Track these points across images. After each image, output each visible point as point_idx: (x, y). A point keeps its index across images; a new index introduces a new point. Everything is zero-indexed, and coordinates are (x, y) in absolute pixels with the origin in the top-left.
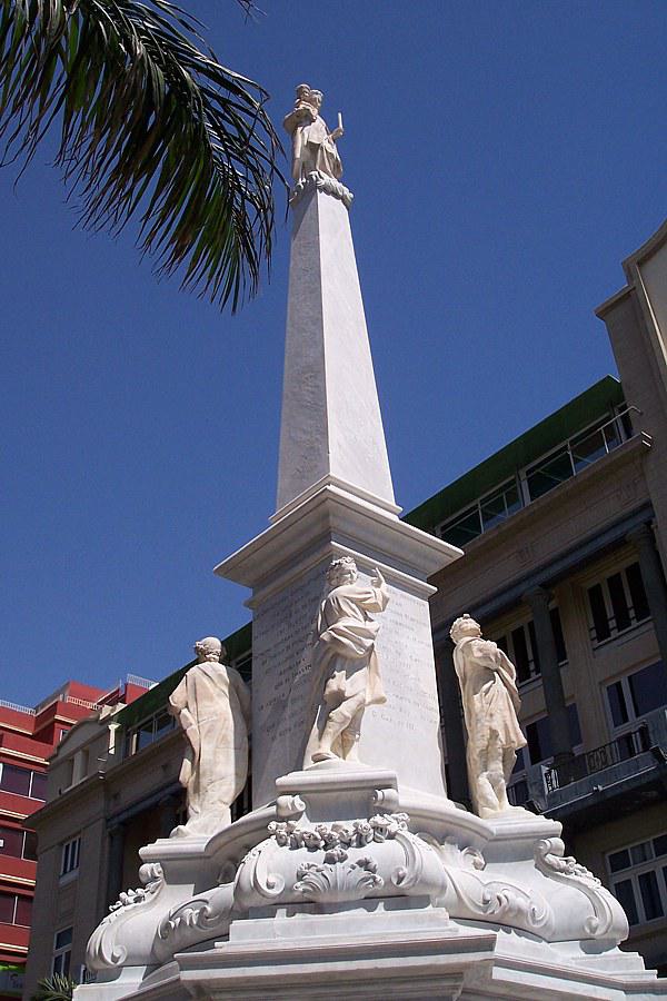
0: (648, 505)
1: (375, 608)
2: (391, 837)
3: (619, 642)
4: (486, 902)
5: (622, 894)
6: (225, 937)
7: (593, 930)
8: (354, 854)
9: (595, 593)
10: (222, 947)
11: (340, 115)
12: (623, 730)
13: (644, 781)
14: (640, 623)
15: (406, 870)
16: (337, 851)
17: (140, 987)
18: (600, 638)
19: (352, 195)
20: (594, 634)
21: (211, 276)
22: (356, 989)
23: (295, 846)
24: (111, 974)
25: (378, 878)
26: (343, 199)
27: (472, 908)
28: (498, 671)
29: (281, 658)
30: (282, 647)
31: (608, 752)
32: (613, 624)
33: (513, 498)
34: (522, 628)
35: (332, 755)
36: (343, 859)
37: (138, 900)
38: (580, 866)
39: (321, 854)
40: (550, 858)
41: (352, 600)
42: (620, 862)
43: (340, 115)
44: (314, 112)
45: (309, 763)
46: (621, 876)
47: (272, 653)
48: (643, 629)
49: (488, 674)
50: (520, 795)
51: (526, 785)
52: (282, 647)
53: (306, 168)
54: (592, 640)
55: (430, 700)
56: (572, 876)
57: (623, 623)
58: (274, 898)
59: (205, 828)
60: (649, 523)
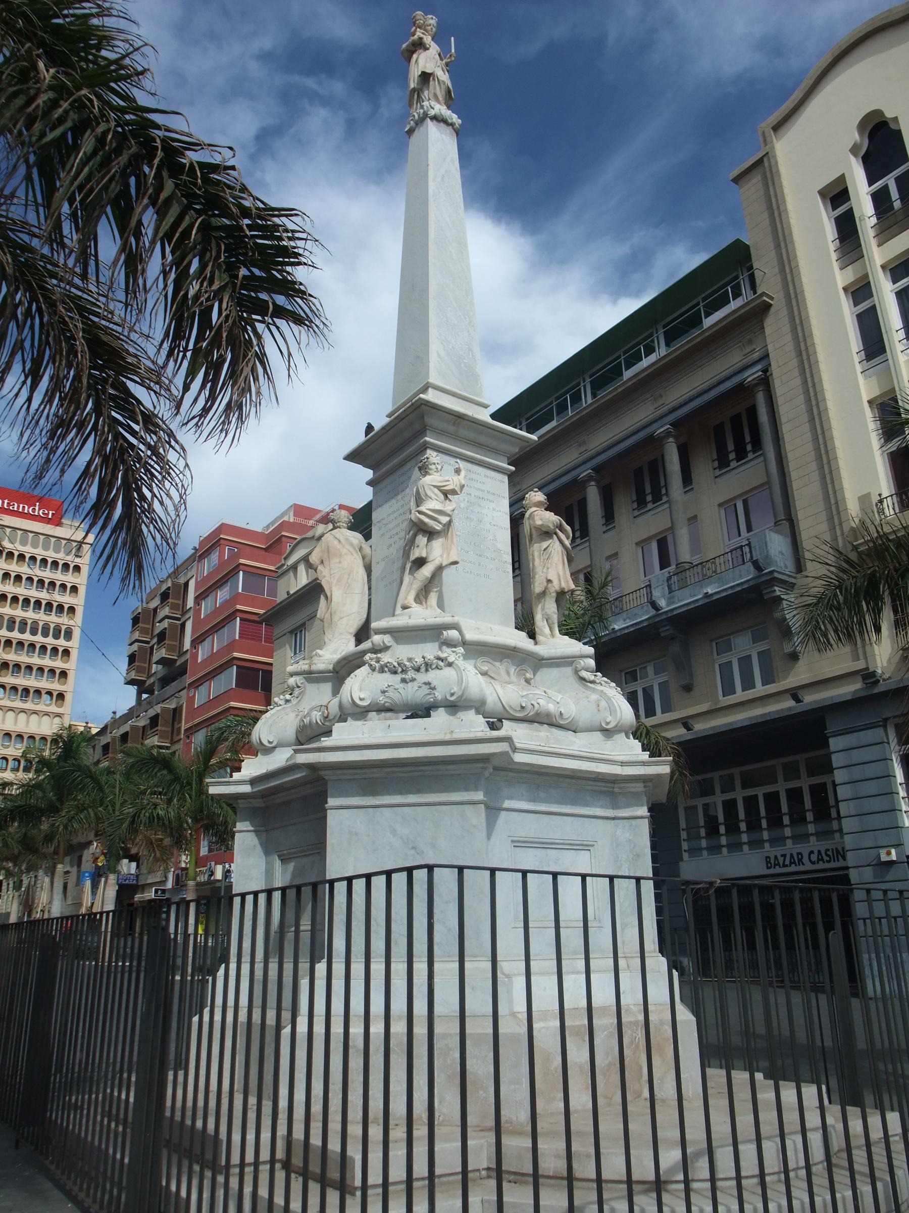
0: (767, 356)
1: (454, 492)
2: (450, 665)
3: (736, 471)
4: (523, 708)
5: (632, 699)
6: (328, 733)
7: (608, 723)
8: (422, 677)
9: (638, 473)
10: (326, 742)
11: (452, 38)
12: (736, 542)
13: (746, 586)
14: (756, 455)
15: (455, 689)
16: (411, 674)
17: (287, 761)
18: (720, 467)
19: (460, 121)
20: (716, 464)
21: (105, 566)
22: (417, 768)
23: (382, 670)
24: (268, 750)
25: (437, 694)
26: (452, 125)
27: (511, 712)
28: (556, 534)
29: (391, 526)
30: (392, 517)
31: (718, 564)
32: (649, 498)
33: (576, 399)
34: (641, 468)
35: (414, 604)
36: (413, 680)
37: (287, 701)
38: (605, 679)
39: (398, 677)
40: (584, 674)
41: (435, 486)
42: (632, 676)
43: (452, 38)
44: (428, 39)
45: (399, 610)
46: (632, 687)
47: (385, 522)
48: (756, 461)
49: (546, 534)
50: (569, 631)
51: (651, 587)
52: (392, 517)
53: (416, 95)
54: (715, 469)
55: (505, 556)
56: (599, 687)
57: (741, 455)
58: (364, 707)
59: (335, 652)
60: (765, 371)
